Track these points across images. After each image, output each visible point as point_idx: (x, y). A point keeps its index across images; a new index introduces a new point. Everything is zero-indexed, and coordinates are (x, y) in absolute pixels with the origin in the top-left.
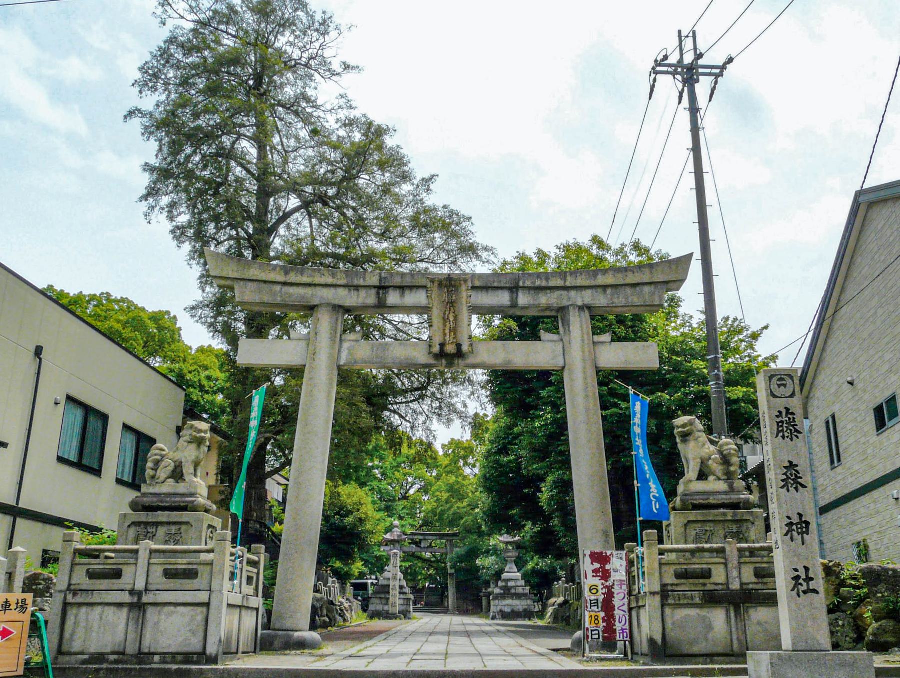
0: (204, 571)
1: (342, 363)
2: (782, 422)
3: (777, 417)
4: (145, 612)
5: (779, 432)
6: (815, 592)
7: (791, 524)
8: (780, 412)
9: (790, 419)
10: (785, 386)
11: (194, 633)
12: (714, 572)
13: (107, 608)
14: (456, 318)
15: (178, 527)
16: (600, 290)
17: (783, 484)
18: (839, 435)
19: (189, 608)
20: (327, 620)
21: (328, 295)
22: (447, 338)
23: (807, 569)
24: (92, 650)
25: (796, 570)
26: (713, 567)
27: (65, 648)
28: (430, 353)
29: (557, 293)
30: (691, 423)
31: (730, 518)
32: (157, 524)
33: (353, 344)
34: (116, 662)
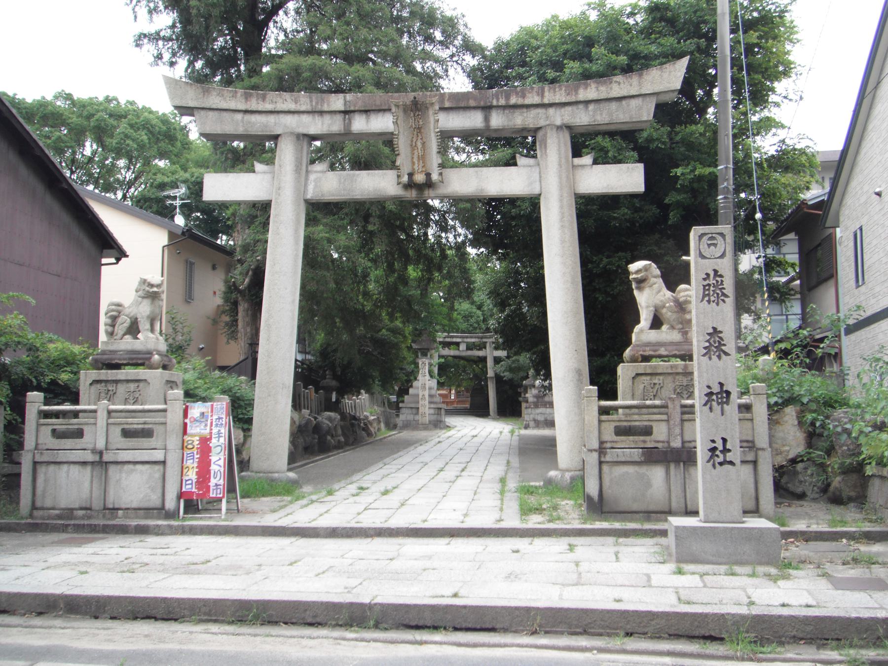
0: (158, 430)
1: (309, 196)
2: (709, 285)
3: (704, 279)
4: (107, 470)
5: (704, 296)
6: (731, 463)
7: (711, 393)
8: (708, 275)
9: (717, 281)
10: (715, 245)
11: (153, 489)
12: (655, 430)
13: (72, 466)
14: (424, 144)
15: (136, 385)
16: (581, 106)
17: (705, 351)
18: (864, 251)
19: (147, 466)
20: (342, 439)
21: (290, 121)
22: (416, 167)
23: (724, 440)
24: (63, 506)
25: (713, 441)
26: (654, 424)
27: (39, 504)
28: (399, 184)
29: (534, 112)
30: (646, 269)
31: (680, 371)
32: (117, 382)
33: (319, 175)
34: (83, 518)
